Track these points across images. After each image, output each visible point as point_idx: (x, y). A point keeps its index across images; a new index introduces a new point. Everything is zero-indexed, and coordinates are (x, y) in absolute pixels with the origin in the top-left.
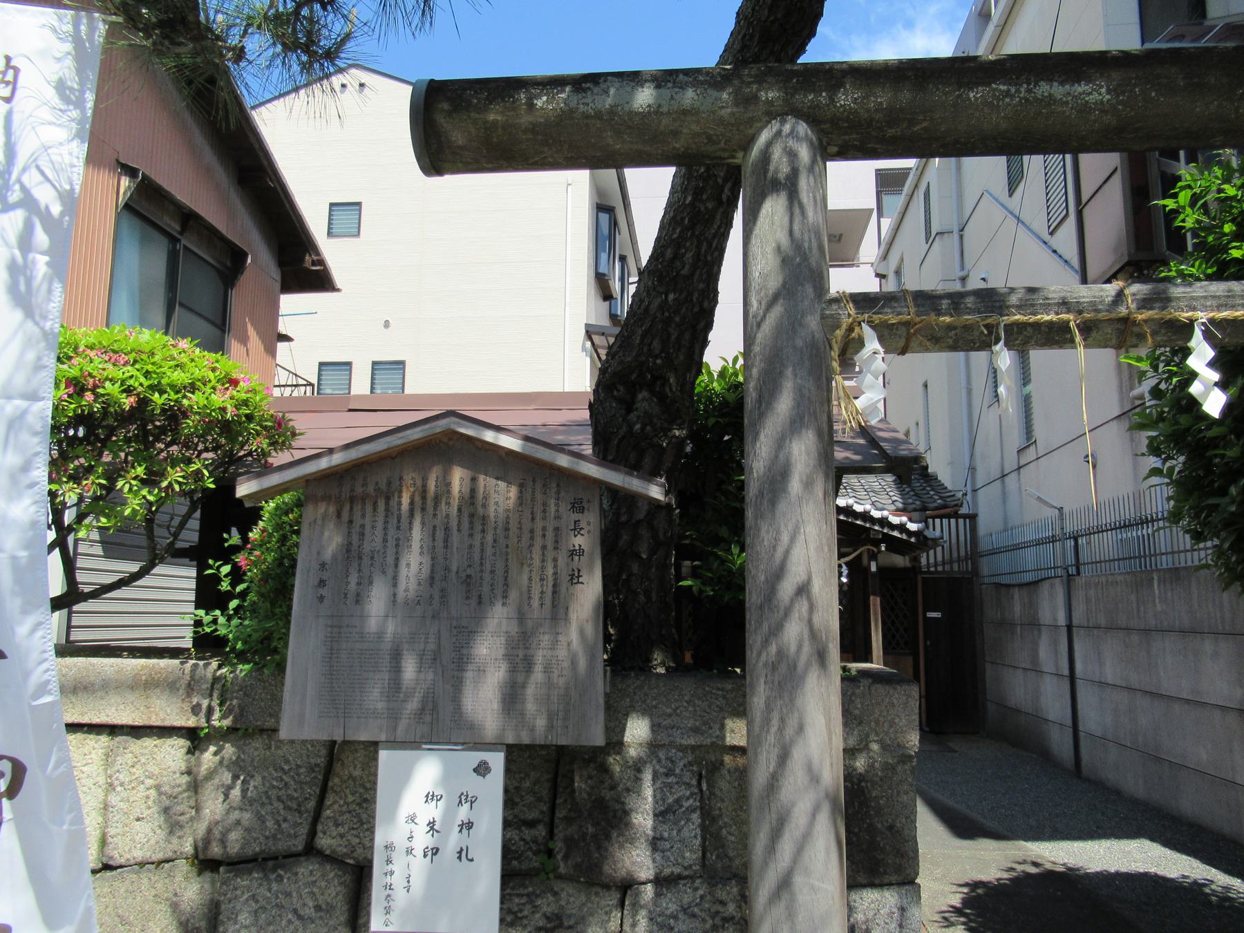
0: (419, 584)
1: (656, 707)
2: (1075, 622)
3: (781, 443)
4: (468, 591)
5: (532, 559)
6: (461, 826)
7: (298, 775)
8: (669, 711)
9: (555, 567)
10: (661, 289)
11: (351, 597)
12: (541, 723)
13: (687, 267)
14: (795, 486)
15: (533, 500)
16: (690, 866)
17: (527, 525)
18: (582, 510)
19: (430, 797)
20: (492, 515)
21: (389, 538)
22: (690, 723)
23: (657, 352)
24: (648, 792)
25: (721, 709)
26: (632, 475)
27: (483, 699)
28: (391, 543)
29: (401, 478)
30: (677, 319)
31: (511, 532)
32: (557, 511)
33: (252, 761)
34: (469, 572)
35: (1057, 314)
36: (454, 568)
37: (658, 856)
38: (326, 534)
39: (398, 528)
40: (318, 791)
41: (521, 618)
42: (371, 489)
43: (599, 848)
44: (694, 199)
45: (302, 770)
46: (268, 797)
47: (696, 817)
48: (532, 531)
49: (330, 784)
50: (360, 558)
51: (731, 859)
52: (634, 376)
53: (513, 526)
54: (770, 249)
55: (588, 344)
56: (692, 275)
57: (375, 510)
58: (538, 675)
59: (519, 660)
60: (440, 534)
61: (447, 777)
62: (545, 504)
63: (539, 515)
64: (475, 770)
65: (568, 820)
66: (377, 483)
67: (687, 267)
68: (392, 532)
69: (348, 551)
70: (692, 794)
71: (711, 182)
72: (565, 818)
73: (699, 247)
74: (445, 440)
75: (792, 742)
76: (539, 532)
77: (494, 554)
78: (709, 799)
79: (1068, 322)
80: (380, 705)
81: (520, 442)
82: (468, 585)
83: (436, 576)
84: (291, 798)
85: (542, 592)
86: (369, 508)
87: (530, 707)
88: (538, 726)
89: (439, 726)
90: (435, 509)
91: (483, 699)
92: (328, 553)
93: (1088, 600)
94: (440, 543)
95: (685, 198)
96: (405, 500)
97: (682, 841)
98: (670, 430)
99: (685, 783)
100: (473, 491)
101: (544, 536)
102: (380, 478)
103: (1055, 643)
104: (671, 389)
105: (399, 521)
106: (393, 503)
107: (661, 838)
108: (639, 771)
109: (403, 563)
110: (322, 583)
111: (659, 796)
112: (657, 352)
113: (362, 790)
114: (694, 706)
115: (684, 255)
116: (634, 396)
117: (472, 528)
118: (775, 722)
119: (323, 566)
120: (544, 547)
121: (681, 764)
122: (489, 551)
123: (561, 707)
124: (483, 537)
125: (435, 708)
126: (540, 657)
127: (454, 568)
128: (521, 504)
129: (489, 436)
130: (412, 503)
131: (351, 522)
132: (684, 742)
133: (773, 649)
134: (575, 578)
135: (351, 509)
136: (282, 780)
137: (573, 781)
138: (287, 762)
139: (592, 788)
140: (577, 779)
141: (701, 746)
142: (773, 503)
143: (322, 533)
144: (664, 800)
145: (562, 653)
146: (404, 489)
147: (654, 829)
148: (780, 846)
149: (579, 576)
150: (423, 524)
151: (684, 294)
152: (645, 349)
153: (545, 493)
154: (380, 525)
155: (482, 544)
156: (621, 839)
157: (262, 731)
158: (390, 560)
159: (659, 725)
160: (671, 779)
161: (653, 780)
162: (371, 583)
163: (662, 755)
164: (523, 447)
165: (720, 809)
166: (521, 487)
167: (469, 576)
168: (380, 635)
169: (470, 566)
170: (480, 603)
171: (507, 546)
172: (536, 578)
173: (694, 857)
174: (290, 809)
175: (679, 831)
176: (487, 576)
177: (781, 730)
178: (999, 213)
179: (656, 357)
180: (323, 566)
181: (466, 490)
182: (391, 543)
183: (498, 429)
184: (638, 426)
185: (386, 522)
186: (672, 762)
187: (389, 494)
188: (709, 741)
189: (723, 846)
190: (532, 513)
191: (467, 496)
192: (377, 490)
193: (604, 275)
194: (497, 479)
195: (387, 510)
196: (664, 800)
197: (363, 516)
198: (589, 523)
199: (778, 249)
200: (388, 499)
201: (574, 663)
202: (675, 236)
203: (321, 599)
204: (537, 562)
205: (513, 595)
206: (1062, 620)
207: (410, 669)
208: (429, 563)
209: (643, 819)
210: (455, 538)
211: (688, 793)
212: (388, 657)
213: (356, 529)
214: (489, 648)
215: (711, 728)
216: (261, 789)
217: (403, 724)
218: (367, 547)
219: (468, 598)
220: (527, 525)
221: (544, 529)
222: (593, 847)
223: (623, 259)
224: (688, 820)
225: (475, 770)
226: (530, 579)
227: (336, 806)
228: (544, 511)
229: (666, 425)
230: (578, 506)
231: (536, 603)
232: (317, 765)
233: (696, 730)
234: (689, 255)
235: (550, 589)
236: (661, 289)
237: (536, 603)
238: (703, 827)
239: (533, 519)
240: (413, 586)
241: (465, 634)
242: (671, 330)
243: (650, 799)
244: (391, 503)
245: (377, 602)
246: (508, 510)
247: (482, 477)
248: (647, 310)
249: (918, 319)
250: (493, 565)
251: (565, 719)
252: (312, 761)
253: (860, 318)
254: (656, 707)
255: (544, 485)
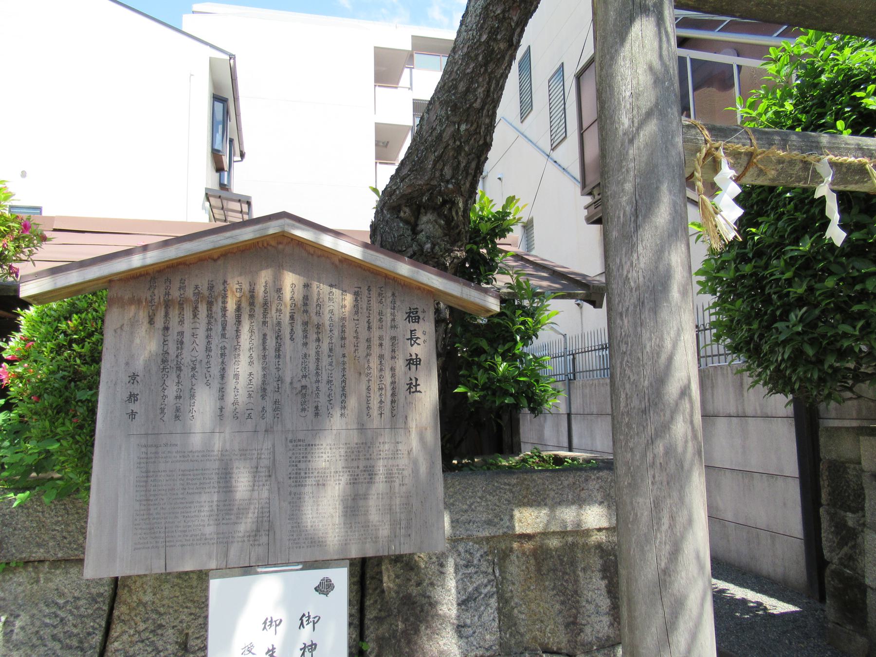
0: (250, 396)
1: (453, 505)
2: (573, 412)
3: (660, 252)
4: (303, 403)
5: (369, 368)
6: (303, 649)
7: (77, 608)
8: (465, 507)
9: (393, 376)
10: (456, 119)
11: (169, 413)
12: (384, 532)
13: (479, 101)
14: (675, 293)
15: (369, 309)
16: (491, 647)
17: (363, 334)
18: (417, 320)
19: (269, 623)
20: (327, 323)
21: (213, 347)
22: (484, 517)
23: (448, 177)
24: (451, 583)
25: (509, 502)
26: (470, 286)
27: (324, 511)
28: (215, 352)
29: (225, 282)
30: (467, 149)
31: (347, 342)
32: (393, 320)
33: (16, 598)
34: (304, 382)
35: (856, 158)
36: (288, 380)
37: (462, 642)
38: (137, 341)
39: (223, 336)
40: (103, 624)
41: (362, 428)
42: (190, 293)
43: (409, 642)
44: (489, 38)
45: (81, 603)
46: (41, 638)
47: (493, 602)
48: (368, 340)
49: (116, 613)
50: (179, 369)
51: (522, 635)
52: (425, 198)
53: (350, 334)
54: (642, 69)
55: (207, 204)
56: (482, 108)
57: (195, 316)
58: (380, 486)
59: (361, 468)
60: (271, 343)
61: (287, 600)
62: (380, 313)
63: (375, 324)
64: (316, 589)
65: (379, 620)
66: (197, 287)
67: (479, 101)
68: (216, 341)
69: (164, 361)
70: (489, 581)
71: (505, 24)
72: (376, 618)
73: (489, 83)
74: (273, 243)
75: (683, 537)
76: (375, 342)
77: (331, 365)
78: (502, 583)
79: (865, 164)
80: (210, 530)
81: (360, 249)
82: (304, 395)
83: (268, 388)
84: (70, 635)
85: (381, 402)
86: (188, 314)
87: (374, 517)
88: (381, 537)
89: (276, 543)
90: (265, 316)
91: (324, 511)
92: (139, 364)
93: (584, 396)
94: (271, 352)
95: (481, 35)
96: (231, 305)
97: (483, 625)
98: (452, 251)
99: (483, 572)
100: (306, 298)
101: (381, 345)
102: (201, 281)
103: (557, 425)
104: (457, 213)
105: (224, 329)
106: (217, 308)
107: (465, 626)
108: (442, 565)
109: (230, 373)
110: (133, 397)
111: (460, 587)
112: (448, 177)
113: (154, 616)
114: (486, 500)
115: (475, 90)
116: (417, 218)
117: (306, 337)
118: (666, 521)
119: (134, 377)
120: (381, 357)
121: (478, 555)
122: (325, 361)
123: (403, 516)
124: (318, 347)
125: (271, 529)
126: (381, 468)
127: (288, 380)
128: (357, 313)
129: (328, 241)
130: (239, 309)
131: (166, 329)
132: (480, 535)
133: (660, 448)
134: (412, 387)
135: (167, 315)
136: (56, 616)
137: (381, 581)
138: (61, 595)
139: (399, 586)
140: (385, 579)
141: (494, 537)
142: (655, 310)
143: (132, 341)
144: (465, 590)
145: (403, 462)
146: (229, 294)
147: (458, 617)
148: (675, 638)
149: (417, 385)
150: (251, 331)
151: (475, 125)
152: (438, 174)
153: (381, 302)
154: (202, 333)
155: (317, 353)
156: (429, 631)
157: (27, 563)
158: (215, 370)
159: (457, 521)
160: (472, 570)
161: (456, 572)
162: (192, 396)
163: (461, 548)
164: (364, 256)
165: (511, 591)
166: (356, 294)
167: (304, 387)
168: (206, 453)
169: (305, 376)
170: (317, 414)
171: (344, 356)
172: (374, 387)
173: (493, 638)
174: (70, 647)
175: (480, 617)
176: (323, 386)
177: (672, 527)
178: (513, 134)
179: (448, 182)
180: (134, 377)
181: (299, 297)
182: (215, 352)
183: (337, 234)
184: (428, 246)
185: (209, 330)
186: (471, 554)
187: (212, 299)
188: (501, 532)
189: (515, 624)
190: (369, 322)
191: (300, 303)
192: (198, 294)
193: (219, 151)
194: (331, 286)
195: (210, 316)
196: (465, 590)
197: (181, 322)
198: (424, 333)
199: (651, 68)
200: (210, 304)
201: (415, 471)
202: (469, 71)
203: (133, 415)
204: (375, 372)
205: (352, 402)
206: (563, 409)
207: (242, 482)
208: (261, 373)
209: (448, 600)
210: (288, 346)
211: (486, 581)
212: (215, 477)
213: (173, 336)
214: (329, 455)
215: (501, 520)
216: (31, 630)
217: (234, 551)
218: (187, 357)
219: (304, 410)
220: (363, 334)
221: (381, 338)
222: (403, 642)
223: (231, 141)
224: (488, 605)
225: (316, 589)
226: (368, 389)
227: (125, 637)
228: (380, 320)
229: (448, 246)
230: (413, 316)
231: (375, 413)
232: (100, 595)
233: (489, 523)
234: (481, 90)
235: (389, 399)
236: (456, 119)
237: (375, 413)
238: (499, 610)
239: (369, 328)
240: (242, 398)
241: (301, 449)
242: (461, 158)
243: (453, 591)
244: (214, 309)
245: (203, 406)
246: (343, 319)
247: (315, 284)
248: (440, 137)
249: (760, 151)
250: (330, 375)
251: (408, 527)
252: (94, 591)
253: (717, 145)
254: (453, 505)
255: (380, 295)
